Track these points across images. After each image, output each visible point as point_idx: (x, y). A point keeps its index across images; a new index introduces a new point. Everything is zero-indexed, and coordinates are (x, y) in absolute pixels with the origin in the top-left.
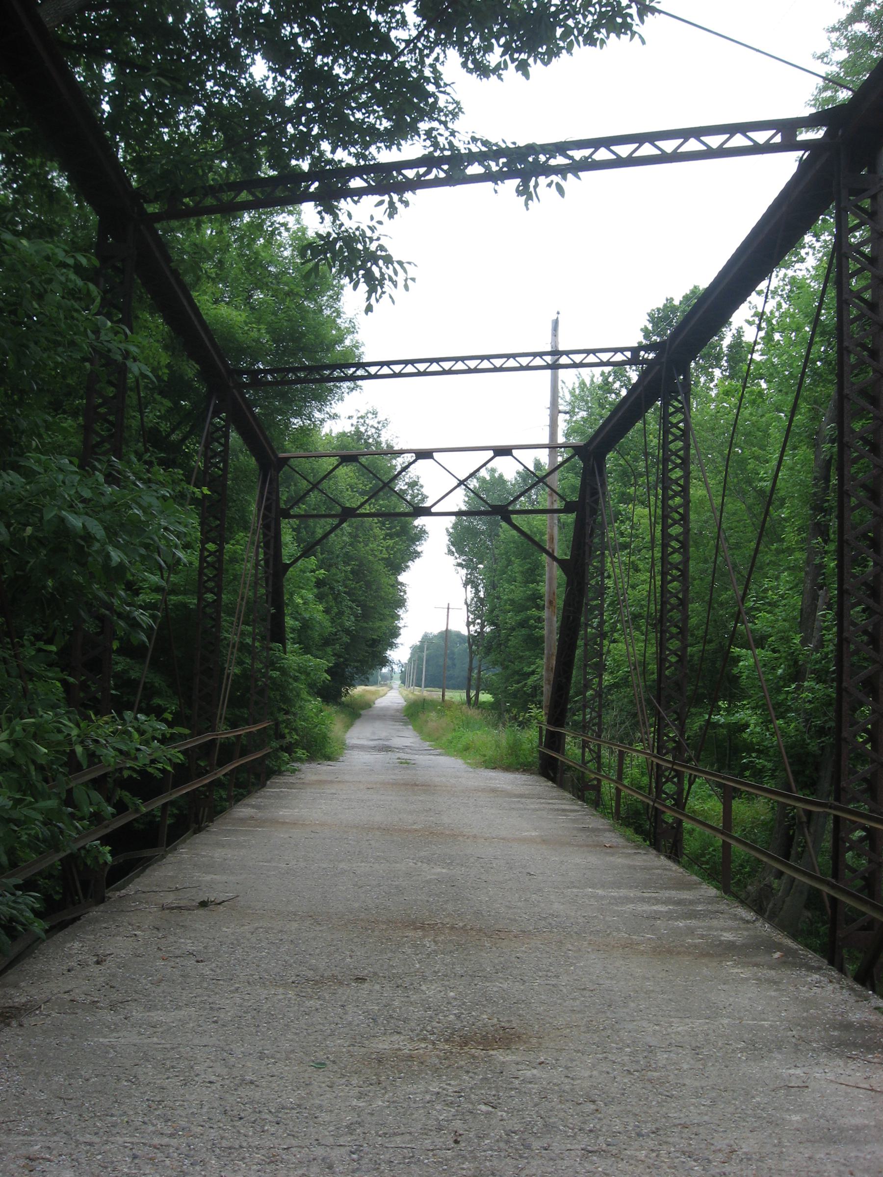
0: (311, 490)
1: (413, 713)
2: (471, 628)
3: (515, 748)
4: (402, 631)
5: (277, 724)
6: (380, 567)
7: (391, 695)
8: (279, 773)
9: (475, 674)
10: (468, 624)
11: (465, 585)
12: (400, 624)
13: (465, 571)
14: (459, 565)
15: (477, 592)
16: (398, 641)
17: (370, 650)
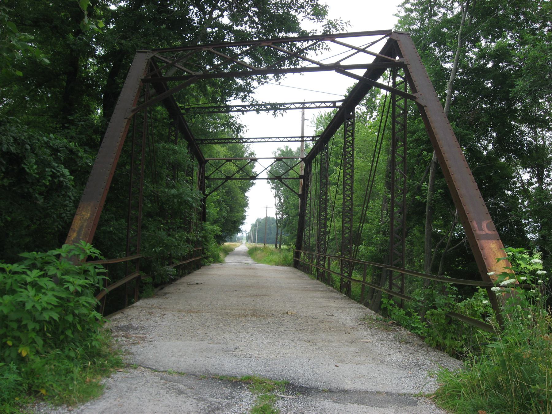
1: (251, 253)
2: (278, 216)
3: (285, 258)
4: (247, 217)
5: (203, 249)
6: (237, 190)
7: (242, 246)
8: (204, 265)
9: (279, 236)
10: (276, 214)
11: (275, 197)
12: (246, 214)
13: (275, 191)
14: (272, 188)
15: (280, 200)
16: (245, 221)
17: (233, 225)
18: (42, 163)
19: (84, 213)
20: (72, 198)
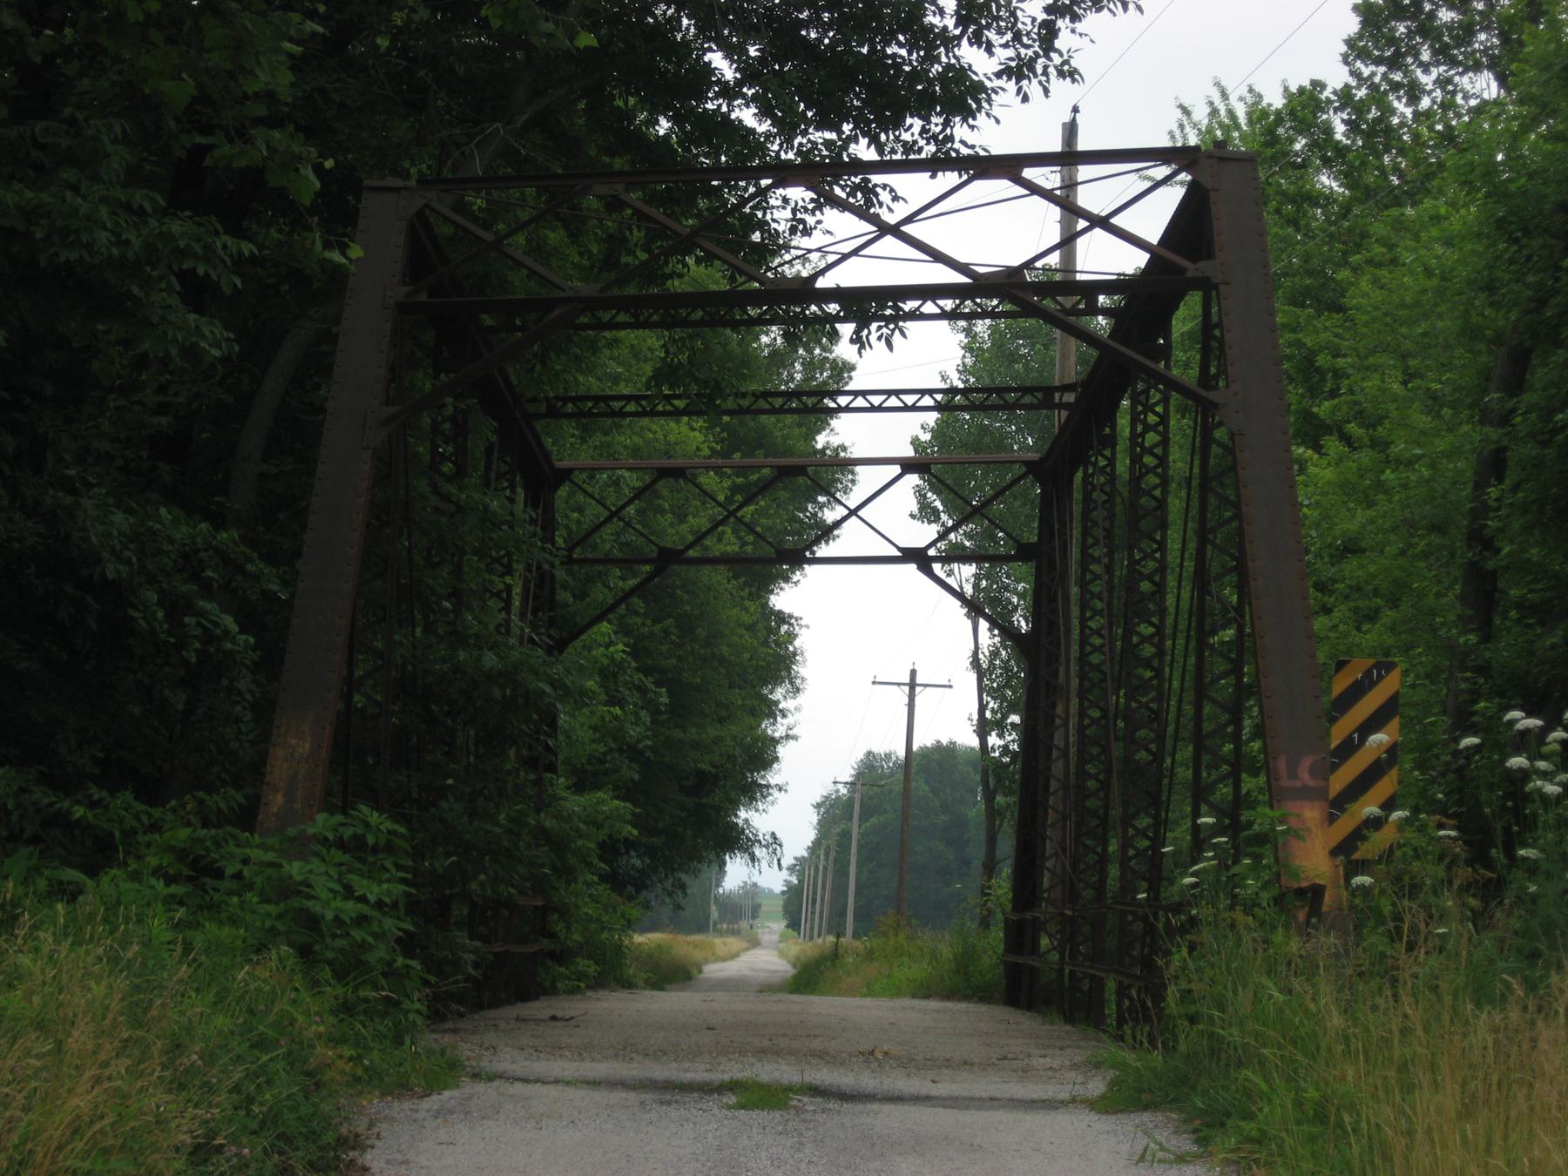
0: (609, 519)
2: (993, 740)
3: (965, 961)
4: (781, 750)
10: (983, 728)
16: (773, 778)
18: (177, 608)
19: (293, 742)
20: (248, 696)
